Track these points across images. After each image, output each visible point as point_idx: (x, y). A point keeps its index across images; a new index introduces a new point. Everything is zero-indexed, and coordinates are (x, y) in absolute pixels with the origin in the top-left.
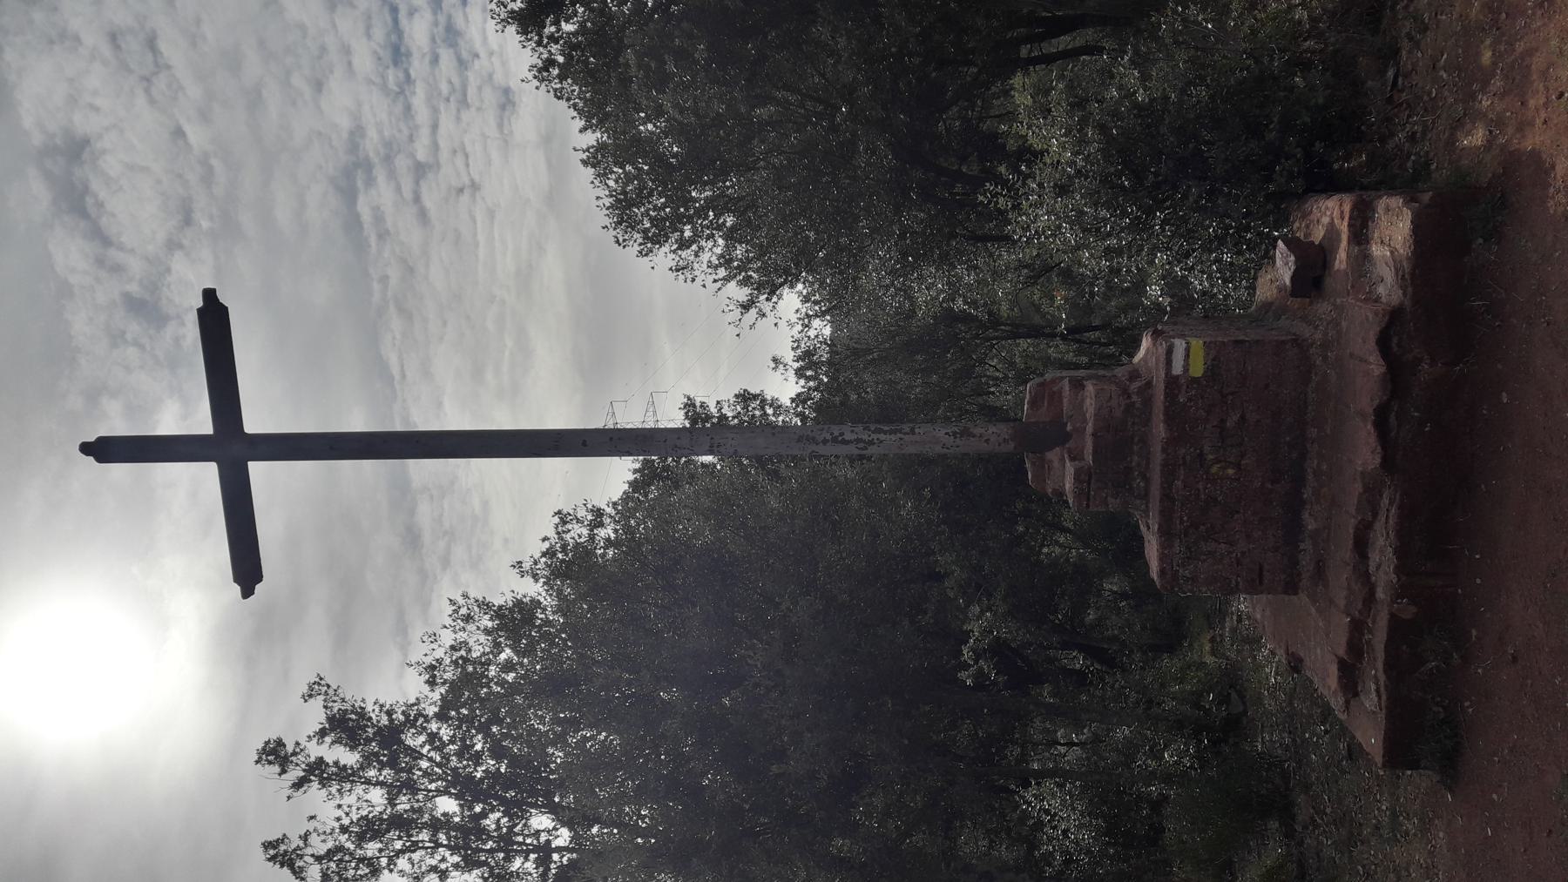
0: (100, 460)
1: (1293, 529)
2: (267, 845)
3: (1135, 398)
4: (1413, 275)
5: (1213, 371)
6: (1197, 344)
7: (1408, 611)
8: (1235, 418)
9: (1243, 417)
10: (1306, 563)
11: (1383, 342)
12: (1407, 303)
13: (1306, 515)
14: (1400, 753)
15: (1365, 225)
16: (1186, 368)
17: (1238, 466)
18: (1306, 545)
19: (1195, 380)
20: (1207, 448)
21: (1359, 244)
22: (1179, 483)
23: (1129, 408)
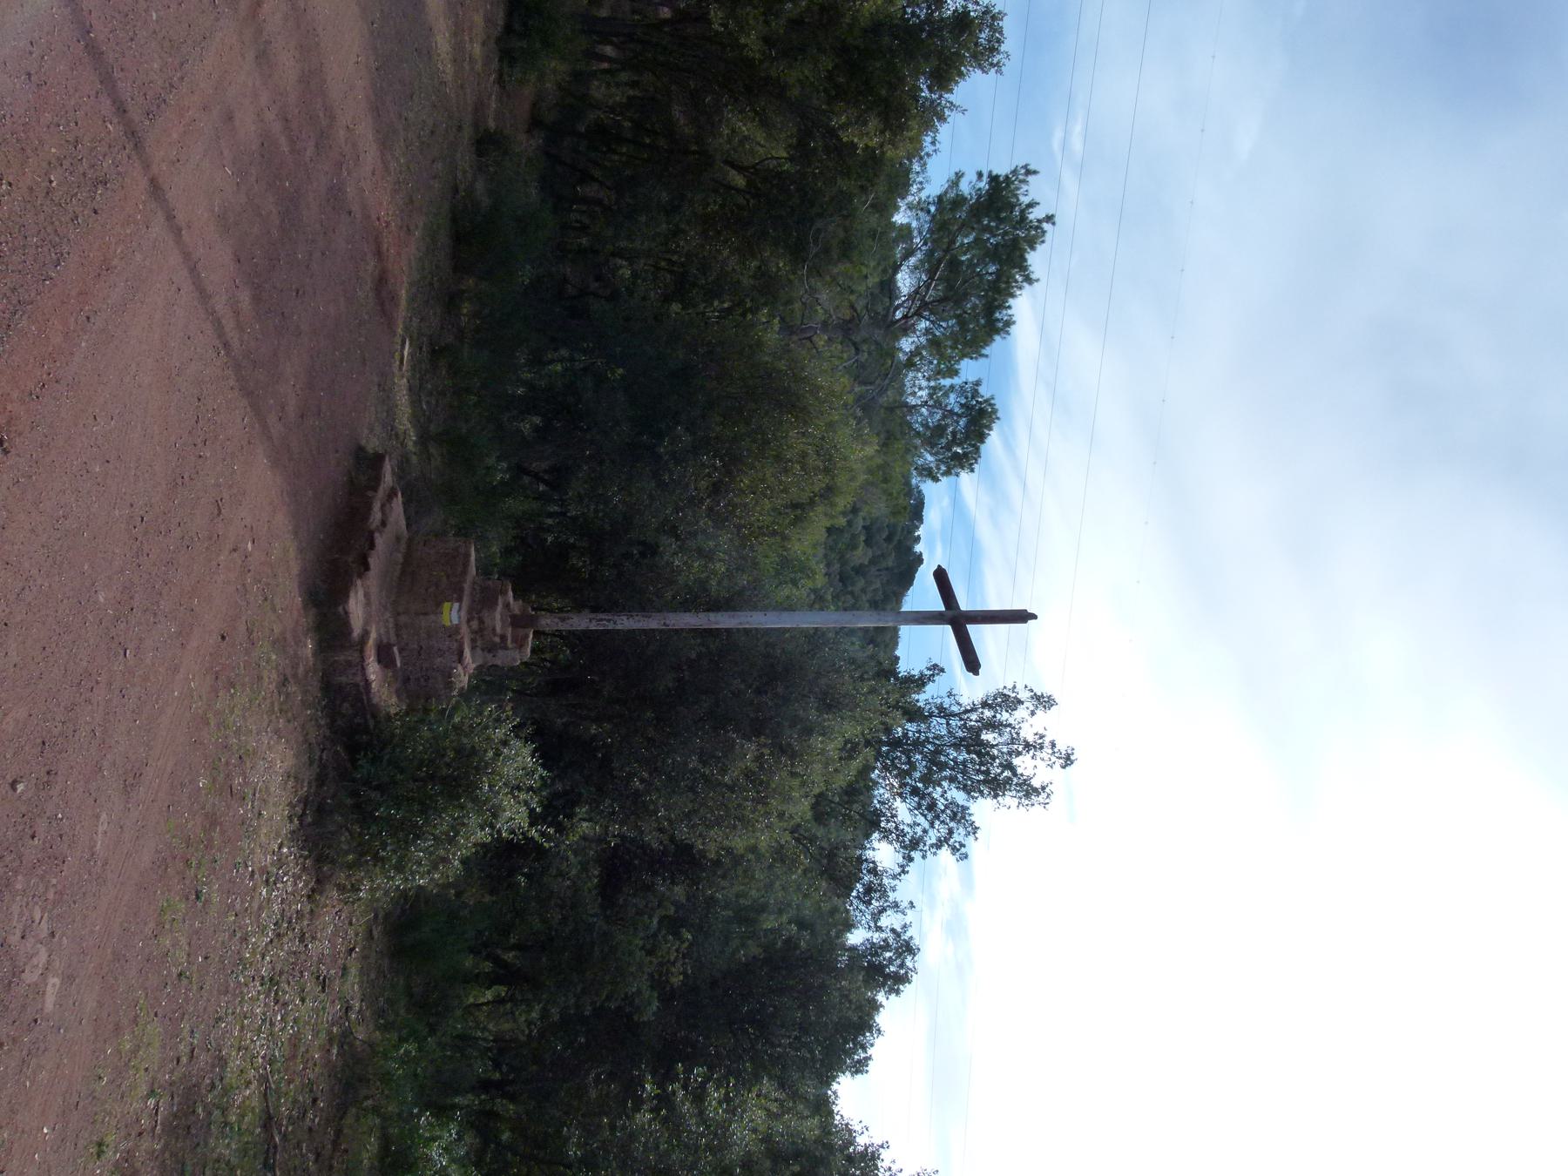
1: (408, 556)
5: (439, 604)
7: (370, 493)
10: (403, 547)
11: (367, 568)
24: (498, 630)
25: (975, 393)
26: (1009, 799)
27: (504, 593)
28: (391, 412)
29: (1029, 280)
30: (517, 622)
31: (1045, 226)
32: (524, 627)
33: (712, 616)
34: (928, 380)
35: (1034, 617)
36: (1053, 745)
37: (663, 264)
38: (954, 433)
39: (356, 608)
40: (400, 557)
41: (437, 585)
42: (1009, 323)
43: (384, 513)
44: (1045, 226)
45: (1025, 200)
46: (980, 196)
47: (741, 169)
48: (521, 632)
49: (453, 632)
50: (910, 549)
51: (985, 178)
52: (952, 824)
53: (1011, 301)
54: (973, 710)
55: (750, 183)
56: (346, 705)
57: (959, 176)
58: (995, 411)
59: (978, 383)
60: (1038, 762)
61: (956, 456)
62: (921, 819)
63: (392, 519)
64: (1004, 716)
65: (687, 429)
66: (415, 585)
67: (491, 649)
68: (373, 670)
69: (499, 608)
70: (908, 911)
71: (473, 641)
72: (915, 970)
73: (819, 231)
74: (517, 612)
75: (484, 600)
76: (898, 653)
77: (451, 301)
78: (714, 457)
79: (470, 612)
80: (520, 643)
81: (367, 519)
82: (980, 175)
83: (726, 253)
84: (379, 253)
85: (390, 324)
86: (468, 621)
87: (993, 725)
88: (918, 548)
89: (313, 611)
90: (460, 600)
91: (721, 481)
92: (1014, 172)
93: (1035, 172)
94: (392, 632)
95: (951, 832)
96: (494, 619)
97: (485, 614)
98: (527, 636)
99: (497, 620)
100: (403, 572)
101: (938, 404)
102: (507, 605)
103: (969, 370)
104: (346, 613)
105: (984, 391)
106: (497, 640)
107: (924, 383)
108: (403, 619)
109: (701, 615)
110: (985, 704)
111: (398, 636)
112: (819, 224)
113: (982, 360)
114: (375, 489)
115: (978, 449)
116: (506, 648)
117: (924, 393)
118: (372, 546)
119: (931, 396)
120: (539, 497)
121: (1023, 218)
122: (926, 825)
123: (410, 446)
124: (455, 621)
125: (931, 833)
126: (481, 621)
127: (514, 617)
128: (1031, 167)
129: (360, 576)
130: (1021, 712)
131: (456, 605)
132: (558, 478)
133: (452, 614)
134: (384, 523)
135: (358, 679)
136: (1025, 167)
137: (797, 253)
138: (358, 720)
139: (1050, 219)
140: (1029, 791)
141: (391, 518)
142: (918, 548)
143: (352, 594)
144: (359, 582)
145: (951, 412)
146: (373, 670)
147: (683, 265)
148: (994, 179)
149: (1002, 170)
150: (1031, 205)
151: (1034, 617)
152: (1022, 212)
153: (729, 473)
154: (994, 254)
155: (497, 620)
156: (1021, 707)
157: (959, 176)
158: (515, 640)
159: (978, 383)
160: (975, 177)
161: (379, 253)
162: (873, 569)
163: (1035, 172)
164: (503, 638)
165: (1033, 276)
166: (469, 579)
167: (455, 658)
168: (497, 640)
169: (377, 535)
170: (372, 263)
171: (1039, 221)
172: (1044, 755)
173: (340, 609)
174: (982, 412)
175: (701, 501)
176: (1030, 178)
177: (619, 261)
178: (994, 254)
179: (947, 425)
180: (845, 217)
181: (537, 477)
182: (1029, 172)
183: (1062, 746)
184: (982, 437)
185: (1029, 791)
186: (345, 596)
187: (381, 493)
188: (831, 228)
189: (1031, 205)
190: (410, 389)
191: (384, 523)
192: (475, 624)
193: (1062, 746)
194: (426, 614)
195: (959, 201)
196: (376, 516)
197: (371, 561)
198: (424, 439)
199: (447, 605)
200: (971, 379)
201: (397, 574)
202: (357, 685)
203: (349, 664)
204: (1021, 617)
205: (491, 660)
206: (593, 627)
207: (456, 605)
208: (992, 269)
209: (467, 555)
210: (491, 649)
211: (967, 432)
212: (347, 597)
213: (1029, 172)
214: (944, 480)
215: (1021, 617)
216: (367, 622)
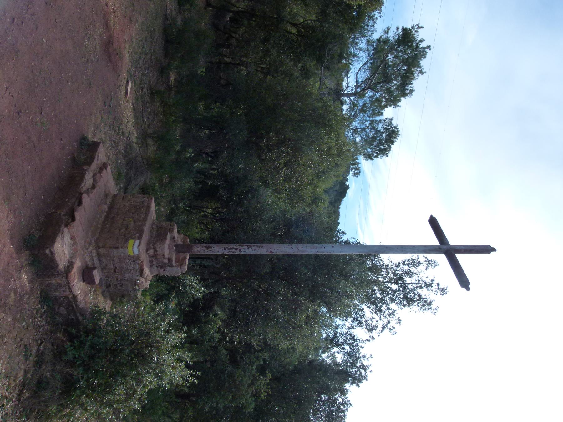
0: (469, 283)
1: (111, 207)
2: (438, 264)
3: (152, 247)
4: (59, 232)
5: (127, 240)
6: (130, 248)
7: (85, 167)
8: (122, 231)
9: (120, 230)
10: (109, 201)
11: (73, 220)
12: (63, 226)
13: (107, 209)
14: (95, 145)
15: (68, 267)
16: (135, 242)
17: (124, 220)
18: (108, 203)
19: (133, 239)
20: (132, 224)
21: (72, 262)
22: (142, 216)
23: (154, 244)
24: (167, 256)
25: (390, 124)
26: (415, 307)
27: (171, 230)
28: (117, 120)
29: (421, 72)
30: (180, 249)
31: (427, 50)
32: (184, 252)
33: (300, 246)
34: (370, 117)
35: (494, 250)
36: (438, 285)
37: (259, 69)
38: (380, 140)
39: (62, 249)
40: (106, 207)
41: (127, 228)
42: (412, 91)
43: (94, 180)
44: (427, 50)
45: (419, 39)
46: (399, 37)
47: (294, 25)
48: (182, 255)
49: (136, 259)
50: (344, 183)
51: (400, 30)
52: (389, 318)
53: (413, 82)
54: (398, 266)
55: (299, 31)
56: (62, 308)
57: (388, 29)
58: (398, 131)
59: (391, 119)
60: (430, 292)
61: (381, 150)
62: (375, 315)
63: (100, 184)
64: (413, 269)
65: (276, 134)
66: (112, 228)
67: (163, 266)
68: (78, 287)
69: (167, 242)
70: (370, 359)
71: (151, 262)
72: (366, 377)
73: (330, 50)
74: (180, 242)
75: (159, 235)
76: (339, 221)
77: (163, 71)
78: (288, 148)
79: (148, 244)
80: (181, 262)
81: (80, 184)
82: (398, 28)
83: (288, 60)
84: (106, 25)
85: (115, 69)
86: (147, 250)
87: (408, 273)
88: (347, 183)
89: (26, 254)
90: (140, 238)
91: (290, 160)
92: (413, 27)
93: (422, 27)
94: (95, 258)
95: (389, 322)
96: (163, 249)
97: (158, 246)
98: (185, 258)
99: (166, 249)
100: (106, 218)
101: (374, 128)
102: (173, 238)
103: (388, 113)
104: (52, 253)
105: (394, 123)
106: (166, 261)
107: (368, 119)
108: (102, 251)
109: (294, 246)
110: (404, 263)
111: (100, 260)
112: (330, 46)
113: (397, 108)
114: (89, 164)
115: (390, 148)
116: (171, 266)
117: (367, 123)
118: (80, 203)
119: (370, 124)
120: (210, 162)
121: (417, 46)
122: (378, 319)
123: (134, 139)
124: (136, 252)
125: (380, 321)
126: (155, 251)
127: (177, 246)
128: (420, 25)
129: (67, 225)
130: (421, 268)
131: (137, 242)
132: (215, 155)
133: (134, 248)
134: (93, 187)
135: (68, 293)
136: (418, 25)
137: (320, 60)
138: (71, 316)
139: (428, 47)
140: (427, 304)
141: (103, 182)
142: (347, 183)
143: (58, 239)
144: (66, 230)
145: (379, 131)
146: (78, 287)
147: (268, 68)
148: (404, 30)
149: (409, 26)
150: (421, 41)
151: (494, 250)
152: (417, 44)
153: (294, 156)
154: (405, 62)
155: (166, 249)
156: (421, 265)
157: (388, 29)
158: (177, 260)
159: (391, 119)
160: (395, 30)
161: (106, 25)
162: (331, 191)
163: (422, 27)
164: (170, 260)
165: (423, 71)
166: (148, 223)
167: (138, 274)
168: (166, 261)
169: (85, 196)
170: (100, 30)
171: (425, 48)
172: (433, 288)
173: (47, 251)
174: (393, 132)
175: (281, 169)
176: (419, 30)
177: (242, 68)
178: (405, 62)
179: (377, 137)
180: (341, 44)
181: (207, 154)
182: (419, 27)
183: (442, 286)
184: (392, 142)
185: (427, 304)
186: (53, 240)
187: (94, 166)
188: (335, 48)
189: (421, 41)
190: (134, 109)
191: (93, 187)
192: (151, 252)
193: (442, 286)
194: (117, 248)
195: (386, 41)
196: (88, 181)
197: (77, 214)
198: (144, 137)
199: (131, 242)
200: (390, 117)
201: (102, 219)
202: (67, 297)
203: (59, 285)
204: (487, 250)
205: (162, 273)
206: (227, 252)
207: (137, 242)
208: (405, 68)
209: (149, 207)
210: (163, 266)
211: (383, 141)
212: (53, 241)
213: (419, 27)
214: (375, 159)
215: (487, 250)
216: (73, 256)
